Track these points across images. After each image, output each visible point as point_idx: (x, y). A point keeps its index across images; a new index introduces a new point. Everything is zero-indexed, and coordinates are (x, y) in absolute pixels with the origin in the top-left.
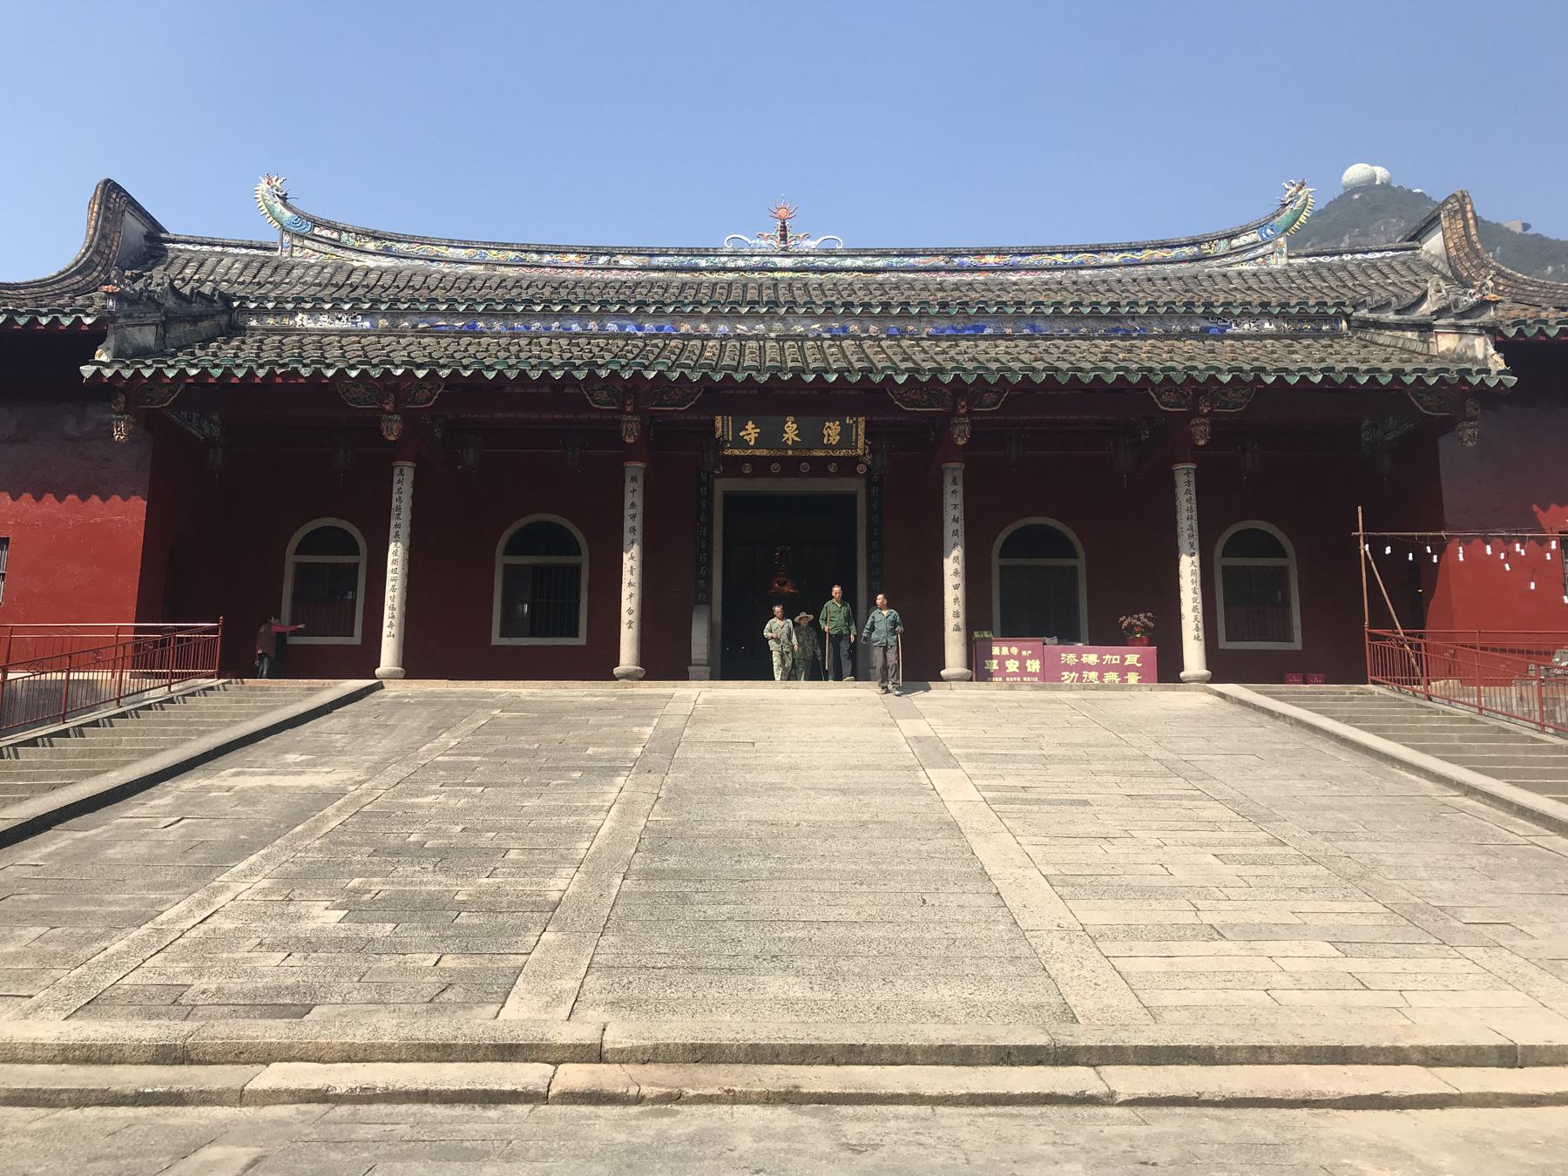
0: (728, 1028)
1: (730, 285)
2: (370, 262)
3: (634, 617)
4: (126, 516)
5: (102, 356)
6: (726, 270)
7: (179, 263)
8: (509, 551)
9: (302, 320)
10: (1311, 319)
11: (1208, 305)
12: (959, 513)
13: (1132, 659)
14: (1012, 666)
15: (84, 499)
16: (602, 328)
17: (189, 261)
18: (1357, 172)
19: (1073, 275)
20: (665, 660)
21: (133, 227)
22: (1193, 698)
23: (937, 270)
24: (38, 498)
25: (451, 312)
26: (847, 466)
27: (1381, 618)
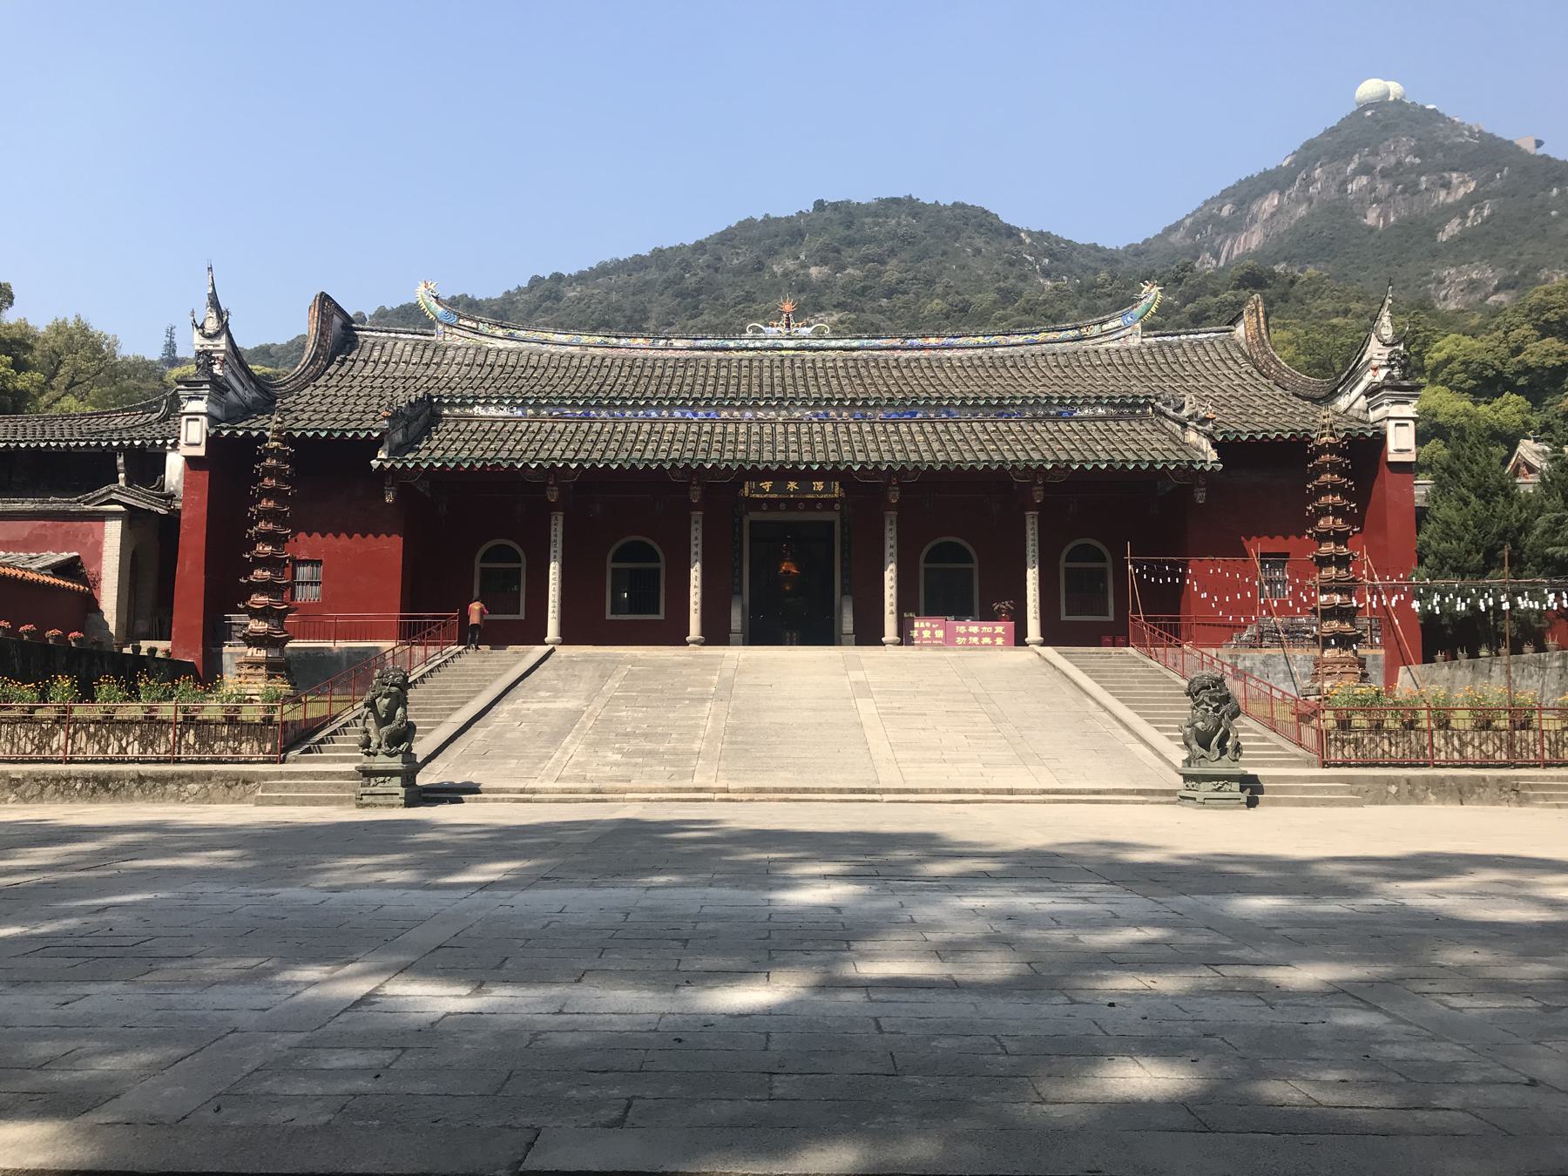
0: (766, 784)
1: (751, 361)
2: (500, 344)
3: (698, 607)
4: (391, 547)
5: (382, 455)
6: (748, 349)
7: (368, 346)
8: (614, 560)
9: (478, 410)
10: (1129, 406)
11: (1061, 398)
12: (893, 542)
13: (999, 629)
14: (926, 634)
15: (364, 536)
16: (671, 415)
17: (374, 345)
18: (1370, 88)
19: (990, 352)
20: (716, 634)
21: (337, 320)
22: (1036, 656)
23: (894, 348)
24: (337, 536)
25: (574, 405)
26: (828, 504)
27: (1136, 611)
